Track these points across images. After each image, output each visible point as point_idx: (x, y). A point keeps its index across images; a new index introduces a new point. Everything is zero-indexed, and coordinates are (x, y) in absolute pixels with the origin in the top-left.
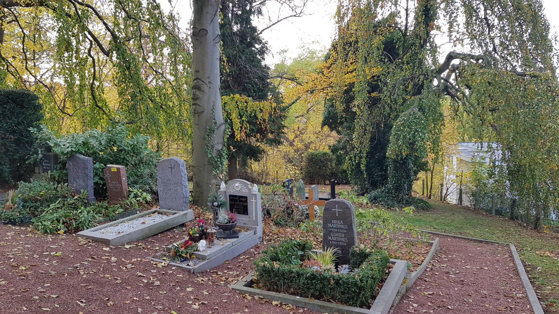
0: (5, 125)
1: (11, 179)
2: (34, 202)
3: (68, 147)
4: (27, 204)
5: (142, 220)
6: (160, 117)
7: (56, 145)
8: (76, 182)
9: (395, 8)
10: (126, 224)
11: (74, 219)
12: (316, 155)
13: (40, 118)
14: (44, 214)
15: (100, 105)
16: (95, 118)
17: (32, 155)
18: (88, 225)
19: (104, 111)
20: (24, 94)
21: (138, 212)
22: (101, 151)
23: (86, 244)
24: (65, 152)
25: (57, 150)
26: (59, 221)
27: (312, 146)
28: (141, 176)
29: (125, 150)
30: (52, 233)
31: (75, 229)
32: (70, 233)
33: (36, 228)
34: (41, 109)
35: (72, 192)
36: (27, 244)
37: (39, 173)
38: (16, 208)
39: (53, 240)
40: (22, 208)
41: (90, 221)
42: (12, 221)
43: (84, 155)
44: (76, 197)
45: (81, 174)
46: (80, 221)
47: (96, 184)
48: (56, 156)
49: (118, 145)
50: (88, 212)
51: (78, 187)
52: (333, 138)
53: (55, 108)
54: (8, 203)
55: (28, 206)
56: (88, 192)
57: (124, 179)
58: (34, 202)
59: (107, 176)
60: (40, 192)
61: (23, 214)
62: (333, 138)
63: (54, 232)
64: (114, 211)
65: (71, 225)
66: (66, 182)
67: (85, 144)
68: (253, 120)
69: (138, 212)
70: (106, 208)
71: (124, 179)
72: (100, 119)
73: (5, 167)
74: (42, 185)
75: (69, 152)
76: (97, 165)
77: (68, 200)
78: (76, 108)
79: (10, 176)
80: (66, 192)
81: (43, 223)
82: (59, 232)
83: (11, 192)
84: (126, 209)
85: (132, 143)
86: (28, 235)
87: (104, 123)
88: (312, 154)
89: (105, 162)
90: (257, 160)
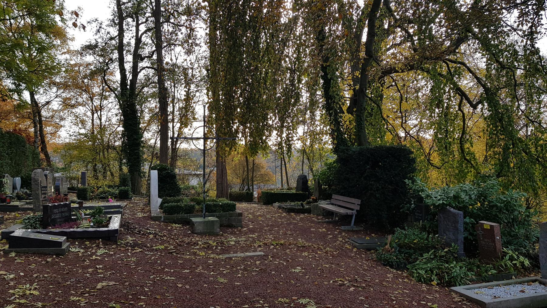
0: (385, 176)
1: (387, 224)
2: (408, 248)
3: (439, 200)
4: (402, 250)
5: (520, 287)
6: (536, 171)
7: (428, 196)
8: (446, 235)
9: (146, 59)
10: (502, 289)
11: (447, 273)
13: (414, 170)
14: (418, 262)
15: (468, 158)
16: (463, 171)
17: (406, 204)
18: (461, 281)
19: (472, 164)
20: (401, 149)
21: (513, 277)
22: (470, 205)
23: (460, 301)
24: (436, 205)
25: (428, 201)
26: (432, 272)
28: (516, 236)
29: (496, 206)
30: (425, 282)
31: (447, 283)
32: (443, 286)
33: (411, 274)
34: (415, 162)
35: (442, 245)
36: (405, 289)
37: (412, 222)
38: (393, 252)
39: (428, 289)
40: (398, 252)
41: (461, 277)
42: (390, 263)
43: (454, 208)
44: (446, 250)
45: (452, 227)
46: (453, 275)
47: (465, 238)
48: (427, 207)
49: (489, 201)
50: (461, 267)
51: (448, 240)
53: (425, 161)
54: (387, 247)
55: (403, 252)
56: (458, 247)
57: (498, 238)
58: (408, 248)
59: (480, 232)
60: (414, 240)
61: (399, 258)
63: (428, 282)
64: (486, 271)
65: (443, 278)
66: (436, 233)
67: (456, 197)
69: (513, 277)
70: (478, 267)
71: (498, 238)
72: (468, 172)
73: (383, 213)
74: (416, 233)
75: (441, 204)
76: (467, 220)
77: (440, 252)
78: (443, 161)
79: (387, 221)
80: (436, 243)
81: (419, 271)
82: (432, 283)
83: (390, 237)
84: (500, 271)
85: (505, 199)
86: (405, 280)
87: (470, 177)
89: (478, 216)
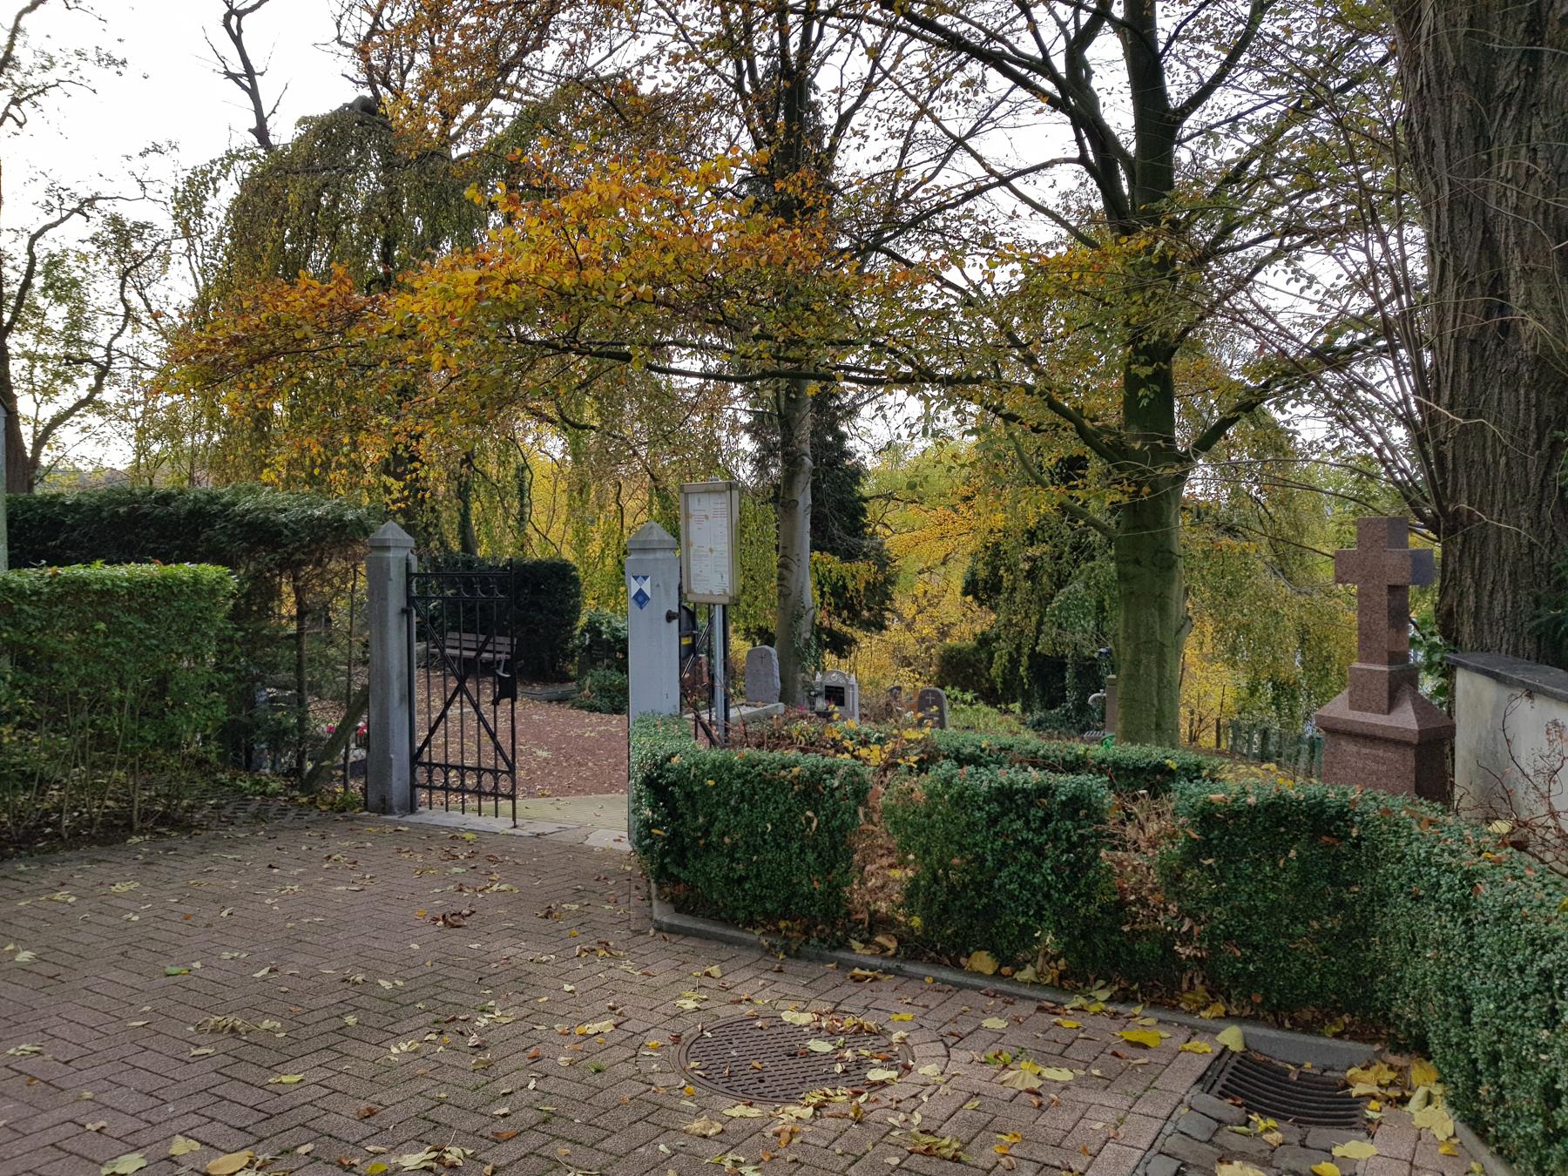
12: (959, 651)
20: (554, 565)
27: (954, 631)
52: (986, 620)
62: (986, 620)
68: (839, 590)
88: (952, 649)
90: (841, 654)
